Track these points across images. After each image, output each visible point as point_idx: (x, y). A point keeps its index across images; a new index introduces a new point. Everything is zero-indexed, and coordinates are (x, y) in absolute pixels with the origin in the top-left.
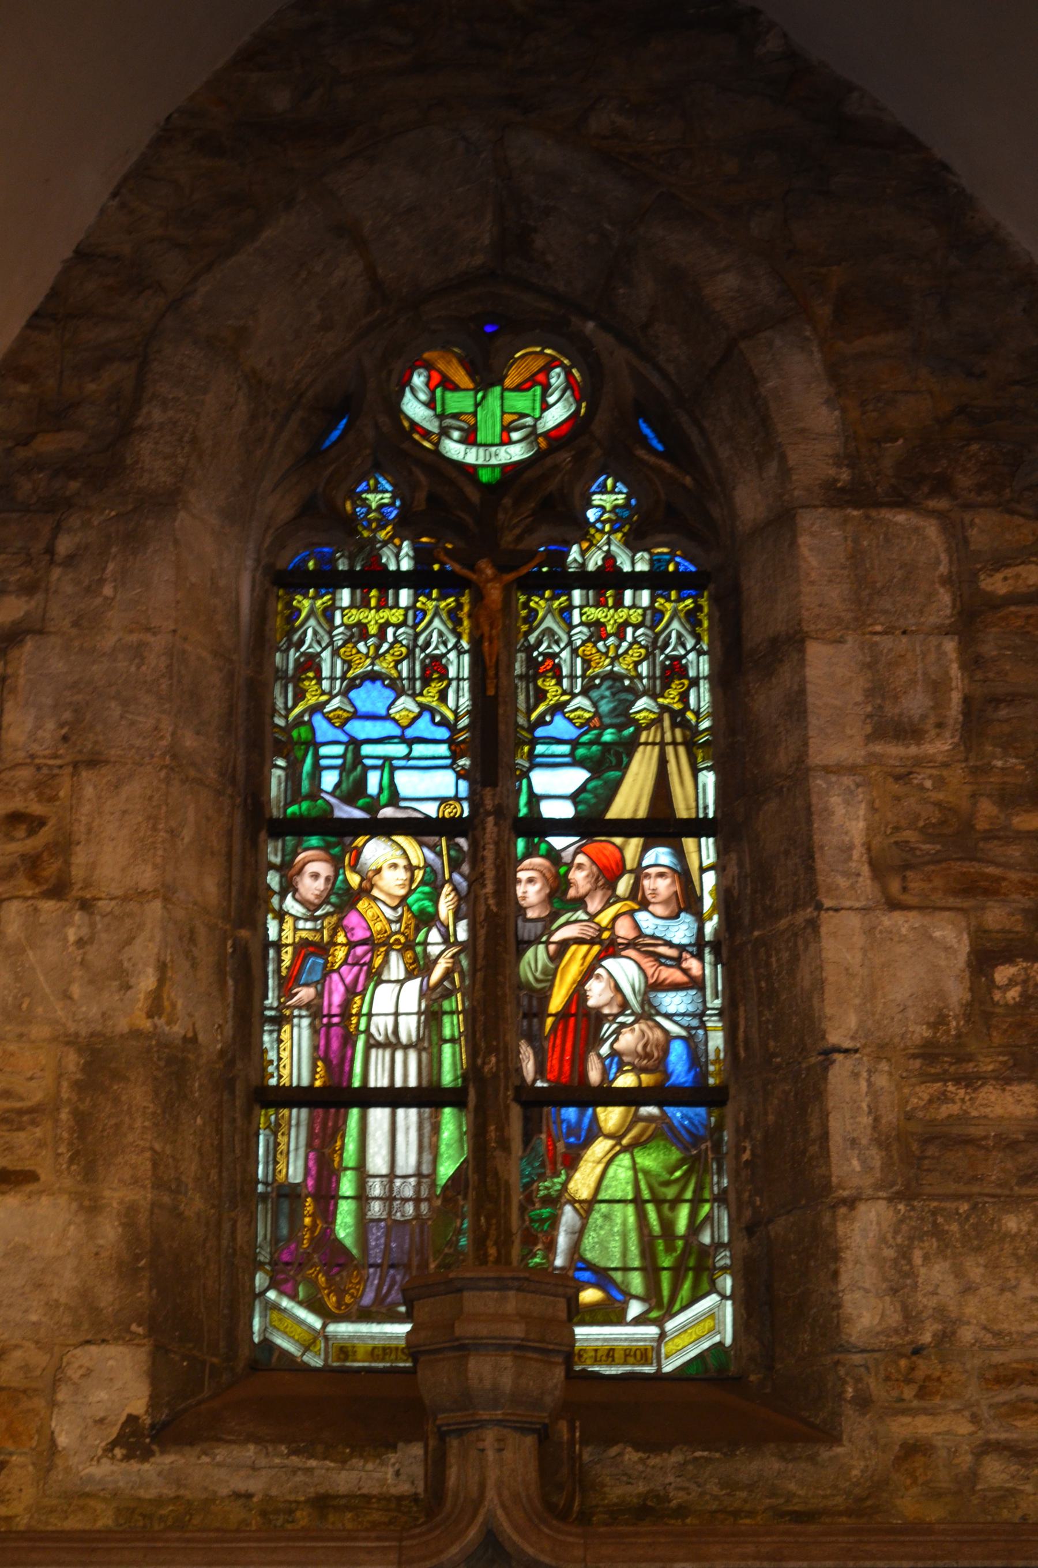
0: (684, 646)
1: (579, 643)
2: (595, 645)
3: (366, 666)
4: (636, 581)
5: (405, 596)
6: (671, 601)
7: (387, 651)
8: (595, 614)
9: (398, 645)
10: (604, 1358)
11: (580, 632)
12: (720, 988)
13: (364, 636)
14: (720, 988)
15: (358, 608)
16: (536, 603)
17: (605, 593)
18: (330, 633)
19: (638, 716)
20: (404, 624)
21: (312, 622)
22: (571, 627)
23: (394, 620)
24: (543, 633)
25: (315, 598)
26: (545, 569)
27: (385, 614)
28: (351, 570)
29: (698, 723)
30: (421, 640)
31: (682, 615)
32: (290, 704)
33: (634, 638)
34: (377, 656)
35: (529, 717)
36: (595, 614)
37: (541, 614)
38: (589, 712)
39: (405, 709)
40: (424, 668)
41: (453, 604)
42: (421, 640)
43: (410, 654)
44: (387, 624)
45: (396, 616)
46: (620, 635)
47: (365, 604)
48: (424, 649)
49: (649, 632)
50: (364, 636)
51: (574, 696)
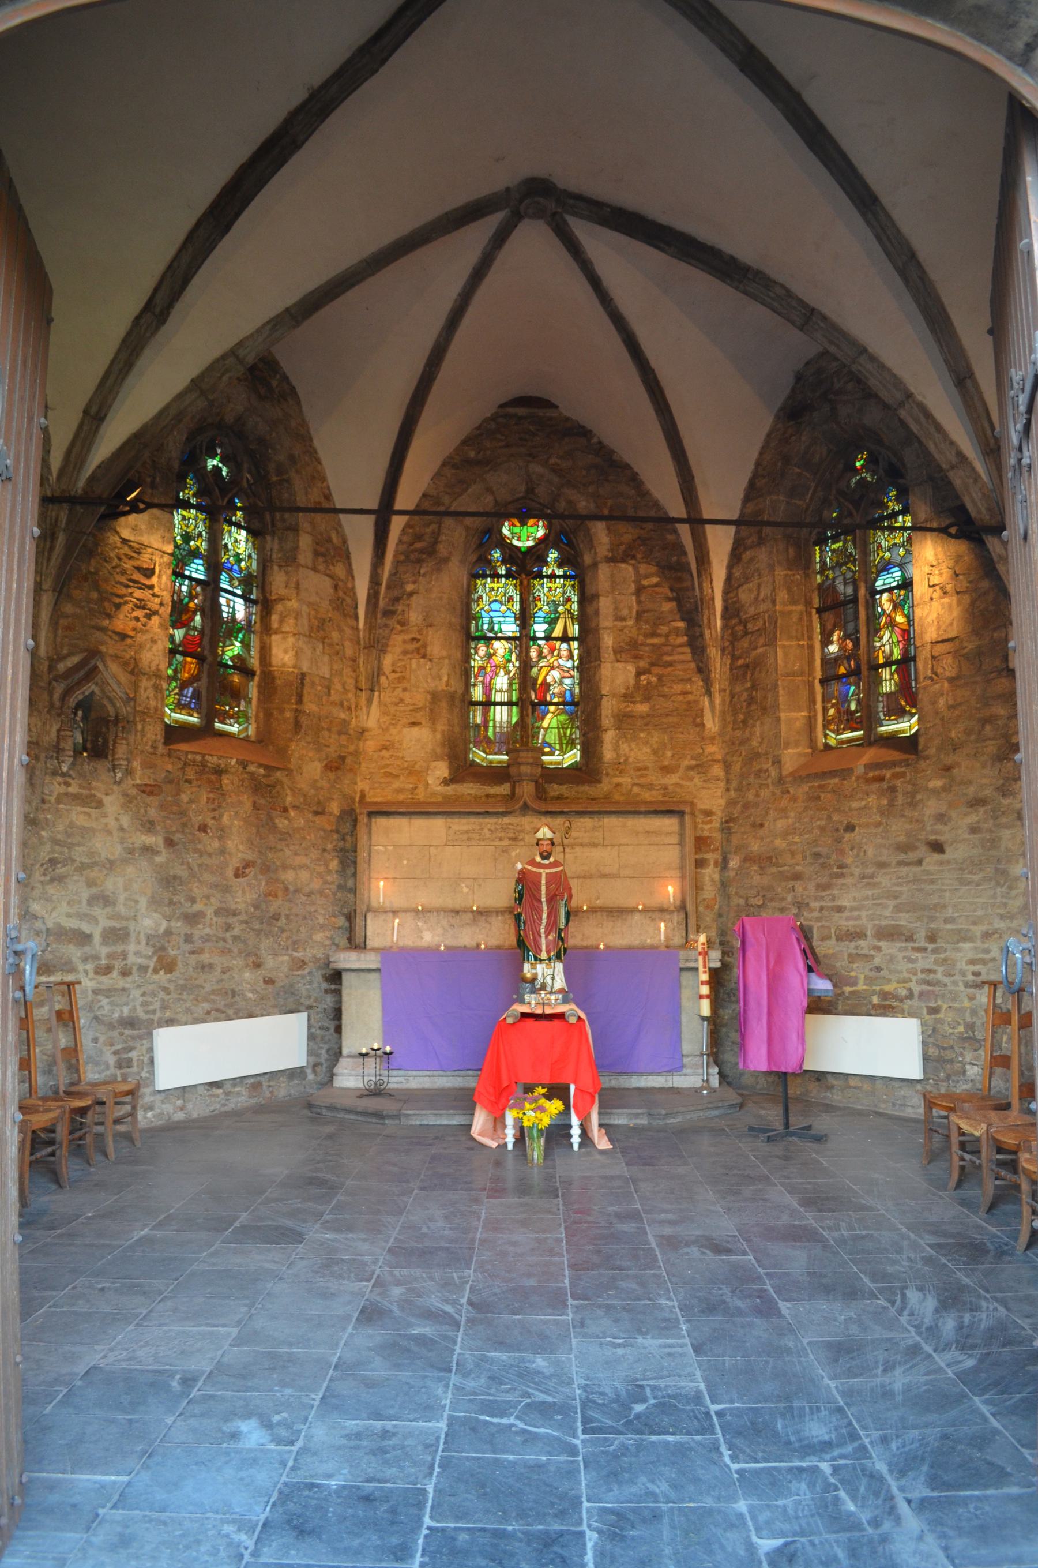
3: (892, 542)
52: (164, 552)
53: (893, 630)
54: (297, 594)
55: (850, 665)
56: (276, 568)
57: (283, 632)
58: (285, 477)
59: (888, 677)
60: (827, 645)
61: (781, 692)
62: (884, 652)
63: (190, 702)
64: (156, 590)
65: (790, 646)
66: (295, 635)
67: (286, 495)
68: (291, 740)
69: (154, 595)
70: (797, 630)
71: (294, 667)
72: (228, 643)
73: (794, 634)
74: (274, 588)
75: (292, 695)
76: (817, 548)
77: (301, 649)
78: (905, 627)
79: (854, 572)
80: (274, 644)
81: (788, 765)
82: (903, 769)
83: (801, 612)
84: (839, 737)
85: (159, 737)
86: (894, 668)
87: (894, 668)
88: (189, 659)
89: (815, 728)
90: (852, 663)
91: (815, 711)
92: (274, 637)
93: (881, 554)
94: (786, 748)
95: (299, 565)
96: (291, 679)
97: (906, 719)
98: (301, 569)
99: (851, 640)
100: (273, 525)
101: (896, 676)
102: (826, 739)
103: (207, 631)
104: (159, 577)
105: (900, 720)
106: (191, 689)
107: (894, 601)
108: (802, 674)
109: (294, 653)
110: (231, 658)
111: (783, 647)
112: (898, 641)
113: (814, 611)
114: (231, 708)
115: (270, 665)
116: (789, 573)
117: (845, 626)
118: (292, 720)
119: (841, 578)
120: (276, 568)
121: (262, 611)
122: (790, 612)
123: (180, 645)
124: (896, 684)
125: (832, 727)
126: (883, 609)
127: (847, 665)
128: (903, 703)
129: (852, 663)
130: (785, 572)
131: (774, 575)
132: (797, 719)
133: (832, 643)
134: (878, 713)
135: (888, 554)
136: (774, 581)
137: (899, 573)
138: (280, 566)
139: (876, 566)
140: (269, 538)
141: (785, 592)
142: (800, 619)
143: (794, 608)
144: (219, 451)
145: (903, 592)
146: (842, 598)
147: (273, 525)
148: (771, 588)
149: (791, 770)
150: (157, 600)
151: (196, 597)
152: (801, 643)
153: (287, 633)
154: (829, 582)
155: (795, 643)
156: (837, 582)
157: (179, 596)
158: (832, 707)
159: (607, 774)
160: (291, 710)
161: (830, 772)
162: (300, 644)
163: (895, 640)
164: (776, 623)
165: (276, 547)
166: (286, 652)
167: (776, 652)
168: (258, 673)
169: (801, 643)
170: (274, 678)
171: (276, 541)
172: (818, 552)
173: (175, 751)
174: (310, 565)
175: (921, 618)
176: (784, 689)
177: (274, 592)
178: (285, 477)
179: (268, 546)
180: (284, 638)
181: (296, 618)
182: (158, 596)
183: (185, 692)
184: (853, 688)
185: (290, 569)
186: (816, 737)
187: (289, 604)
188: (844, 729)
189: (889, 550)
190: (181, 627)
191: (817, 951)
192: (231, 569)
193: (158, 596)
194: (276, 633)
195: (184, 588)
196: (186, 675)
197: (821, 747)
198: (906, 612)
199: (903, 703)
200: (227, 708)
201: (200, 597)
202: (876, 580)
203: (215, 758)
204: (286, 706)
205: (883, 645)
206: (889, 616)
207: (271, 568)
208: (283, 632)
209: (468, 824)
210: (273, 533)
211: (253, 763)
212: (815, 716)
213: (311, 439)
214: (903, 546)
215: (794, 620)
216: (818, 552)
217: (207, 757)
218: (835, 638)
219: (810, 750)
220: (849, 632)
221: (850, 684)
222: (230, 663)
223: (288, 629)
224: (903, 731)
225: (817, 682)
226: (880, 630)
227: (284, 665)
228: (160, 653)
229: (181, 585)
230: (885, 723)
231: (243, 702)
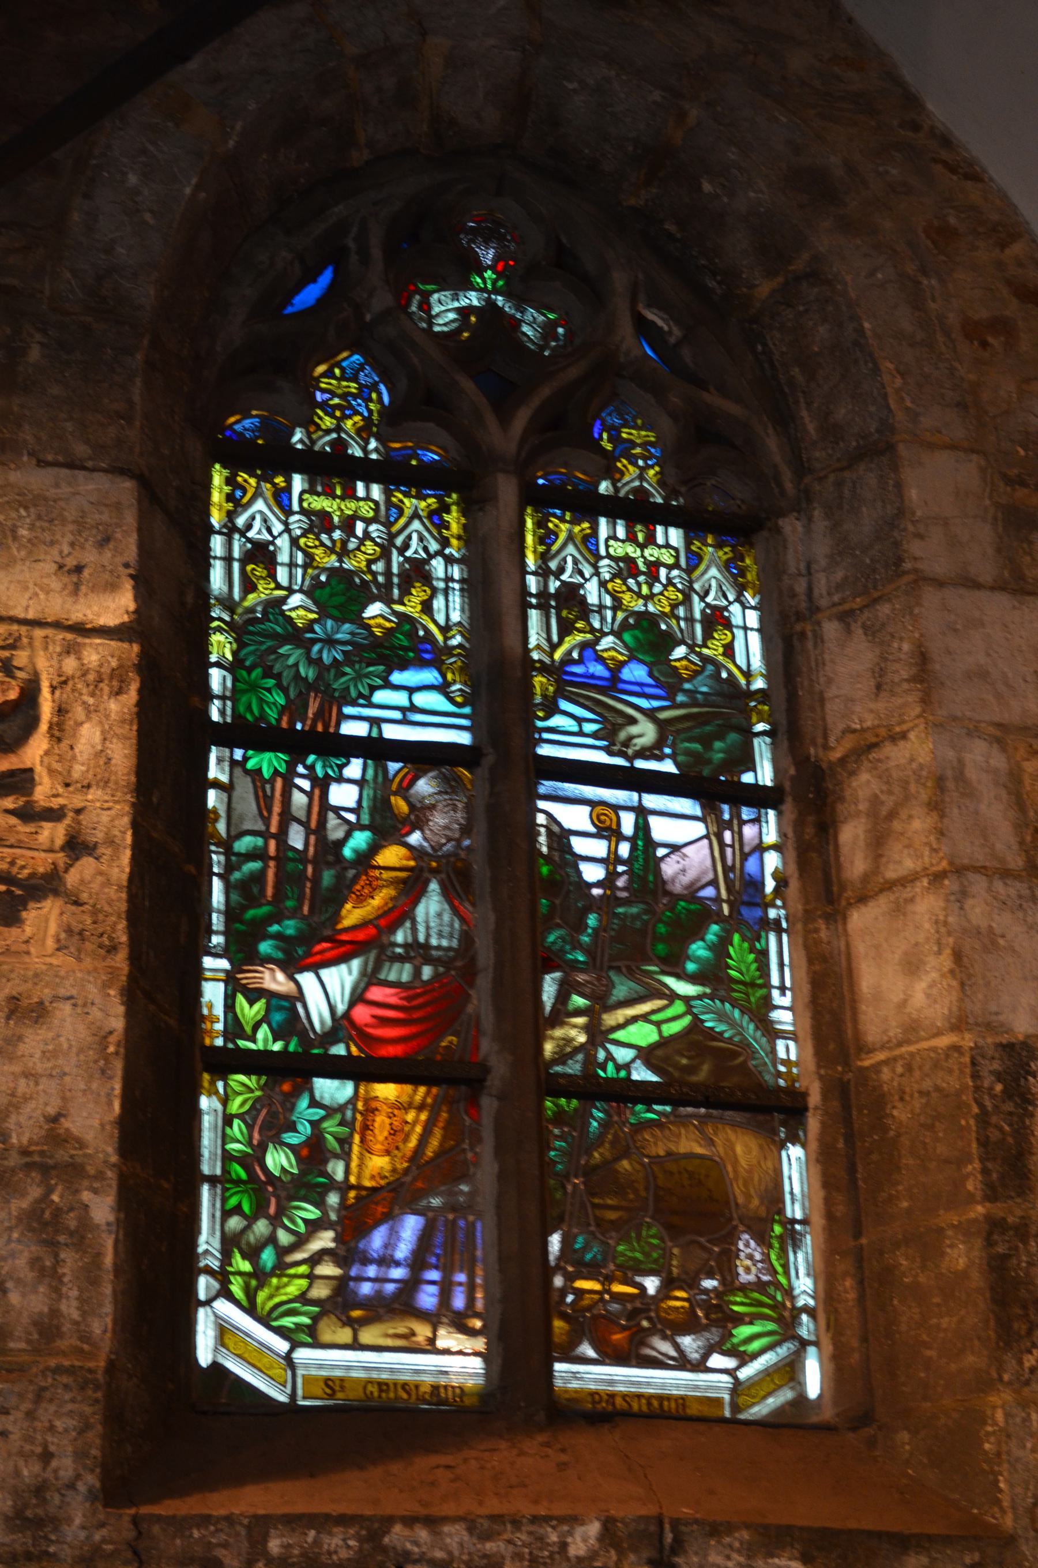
0: (269, 530)
4: (368, 471)
7: (358, 549)
8: (320, 503)
11: (609, 566)
12: (786, 960)
13: (634, 572)
14: (786, 960)
17: (634, 527)
18: (595, 567)
19: (372, 622)
20: (676, 565)
21: (571, 549)
22: (289, 512)
26: (260, 442)
28: (667, 504)
29: (749, 683)
30: (399, 541)
31: (578, 540)
32: (555, 638)
33: (669, 579)
35: (551, 655)
36: (320, 503)
38: (390, 621)
42: (399, 541)
46: (653, 576)
47: (330, 494)
48: (402, 551)
49: (685, 576)
50: (634, 572)
51: (291, 591)
52: (81, 629)
54: (926, 700)
56: (831, 629)
57: (889, 886)
58: (799, 265)
63: (411, 1285)
64: (43, 793)
66: (938, 878)
67: (823, 330)
68: (985, 1384)
69: (28, 814)
71: (959, 1024)
72: (622, 989)
74: (833, 708)
75: (965, 1158)
77: (990, 941)
80: (860, 948)
85: (65, 1466)
88: (387, 1091)
92: (859, 919)
95: (921, 579)
96: (951, 1082)
98: (931, 597)
100: (801, 468)
103: (485, 954)
104: (58, 732)
106: (411, 1226)
109: (946, 961)
110: (647, 1055)
114: (668, 1284)
115: (863, 1048)
118: (977, 1281)
120: (831, 629)
121: (799, 824)
123: (331, 1036)
138: (845, 617)
140: (791, 526)
144: (488, 256)
147: (801, 468)
150: (52, 833)
151: (418, 818)
153: (905, 881)
157: (317, 830)
160: (965, 1230)
162: (978, 911)
165: (821, 549)
166: (912, 966)
168: (814, 1099)
170: (879, 1103)
171: (820, 524)
173: (180, 1525)
174: (986, 570)
177: (836, 727)
178: (799, 265)
179: (792, 561)
180: (899, 910)
181: (936, 807)
182: (54, 815)
183: (377, 1240)
185: (884, 610)
187: (896, 755)
190: (343, 958)
191: (621, 999)
192: (613, 683)
193: (54, 815)
194: (863, 899)
195: (343, 795)
196: (379, 1163)
200: (652, 1284)
201: (439, 820)
203: (455, 1536)
204: (950, 1218)
207: (819, 639)
208: (889, 886)
210: (803, 503)
211: (716, 1530)
213: (911, 101)
217: (397, 1536)
222: (641, 1074)
223: (909, 864)
227: (912, 1029)
228: (69, 1064)
229: (322, 785)
231: (747, 1246)
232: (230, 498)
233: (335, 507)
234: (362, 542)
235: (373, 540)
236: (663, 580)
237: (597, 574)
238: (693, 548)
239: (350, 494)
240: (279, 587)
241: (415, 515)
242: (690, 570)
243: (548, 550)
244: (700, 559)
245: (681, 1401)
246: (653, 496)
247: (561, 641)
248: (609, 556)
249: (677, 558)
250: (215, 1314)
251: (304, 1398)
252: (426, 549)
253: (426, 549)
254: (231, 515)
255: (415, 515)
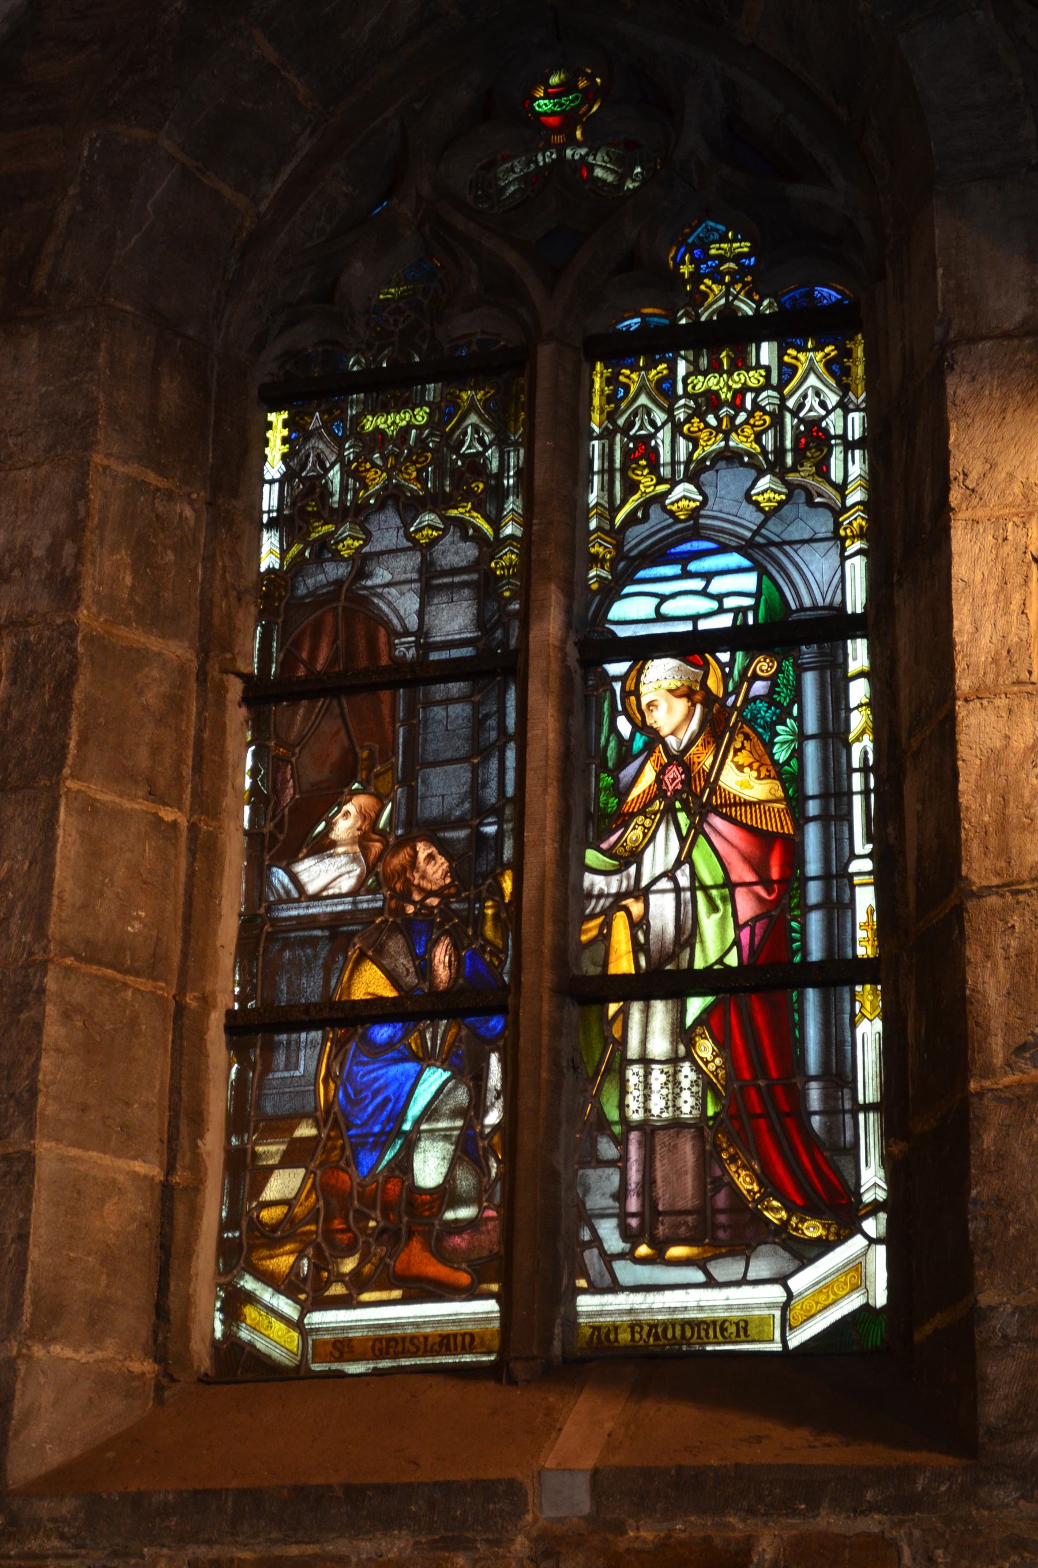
1: (682, 417)
2: (703, 420)
3: (714, 444)
5: (767, 352)
6: (640, 369)
7: (746, 422)
8: (700, 384)
9: (758, 414)
10: (436, 1347)
11: (768, 396)
15: (705, 374)
16: (628, 377)
18: (670, 411)
20: (767, 386)
23: (753, 383)
24: (635, 414)
25: (647, 368)
27: (738, 379)
30: (791, 403)
34: (734, 428)
35: (612, 521)
37: (633, 389)
38: (694, 500)
39: (685, 498)
40: (626, 453)
41: (665, 372)
42: (791, 403)
43: (777, 421)
44: (745, 389)
45: (754, 379)
46: (737, 405)
47: (715, 367)
51: (674, 483)
53: (698, 829)
55: (426, 969)
59: (660, 1046)
60: (289, 858)
61: (53, 1031)
62: (639, 925)
65: (117, 815)
70: (156, 750)
73: (142, 758)
76: (277, 418)
78: (778, 823)
79: (490, 547)
81: (39, 1429)
82: (872, 1524)
83: (182, 670)
84: (318, 1318)
86: (695, 1006)
87: (695, 1006)
89: (189, 1254)
90: (441, 956)
91: (197, 1166)
93: (647, 485)
94: (42, 1333)
97: (759, 1268)
99: (444, 848)
101: (705, 1048)
102: (233, 1315)
105: (727, 1269)
107: (709, 699)
108: (153, 969)
111: (90, 809)
112: (729, 884)
113: (235, 688)
116: (152, 478)
117: (409, 780)
119: (408, 564)
122: (138, 658)
124: (705, 1084)
125: (282, 1262)
126: (640, 726)
127: (404, 963)
128: (745, 1183)
129: (441, 956)
130: (133, 470)
131: (83, 468)
132: (111, 1188)
133: (323, 847)
134: (588, 1218)
135: (685, 489)
136: (81, 493)
137: (749, 582)
139: (617, 535)
141: (124, 556)
142: (175, 704)
143: (154, 643)
145: (763, 665)
146: (406, 650)
148: (60, 519)
149: (54, 1457)
152: (168, 815)
154: (335, 571)
155: (140, 805)
156: (381, 576)
158: (287, 1161)
159: (303, 1107)
161: (355, 1493)
163: (709, 872)
164: (65, 684)
167: (51, 822)
169: (168, 815)
172: (277, 434)
175: (995, 759)
176: (66, 1015)
184: (434, 1079)
186: (188, 1302)
188: (359, 1282)
189: (692, 477)
197: (203, 1361)
198: (781, 754)
199: (745, 1183)
202: (612, 592)
205: (642, 893)
206: (679, 759)
209: (543, 878)
212: (196, 1187)
214: (776, 467)
215: (151, 697)
216: (277, 434)
218: (344, 826)
219: (144, 1367)
220: (431, 808)
221: (425, 1059)
224: (743, 1328)
225: (216, 1020)
226: (624, 820)
230: (626, 1272)
232: (611, 398)
233: (722, 384)
234: (751, 414)
235: (762, 409)
236: (748, 405)
237: (671, 418)
238: (786, 359)
239: (740, 363)
240: (661, 481)
241: (811, 369)
242: (779, 388)
243: (617, 407)
244: (795, 369)
245: (742, 1324)
246: (630, 326)
247: (624, 502)
248: (686, 395)
249: (768, 377)
250: (865, 1254)
251: (313, 1341)
252: (823, 404)
253: (823, 404)
254: (612, 417)
255: (811, 369)
